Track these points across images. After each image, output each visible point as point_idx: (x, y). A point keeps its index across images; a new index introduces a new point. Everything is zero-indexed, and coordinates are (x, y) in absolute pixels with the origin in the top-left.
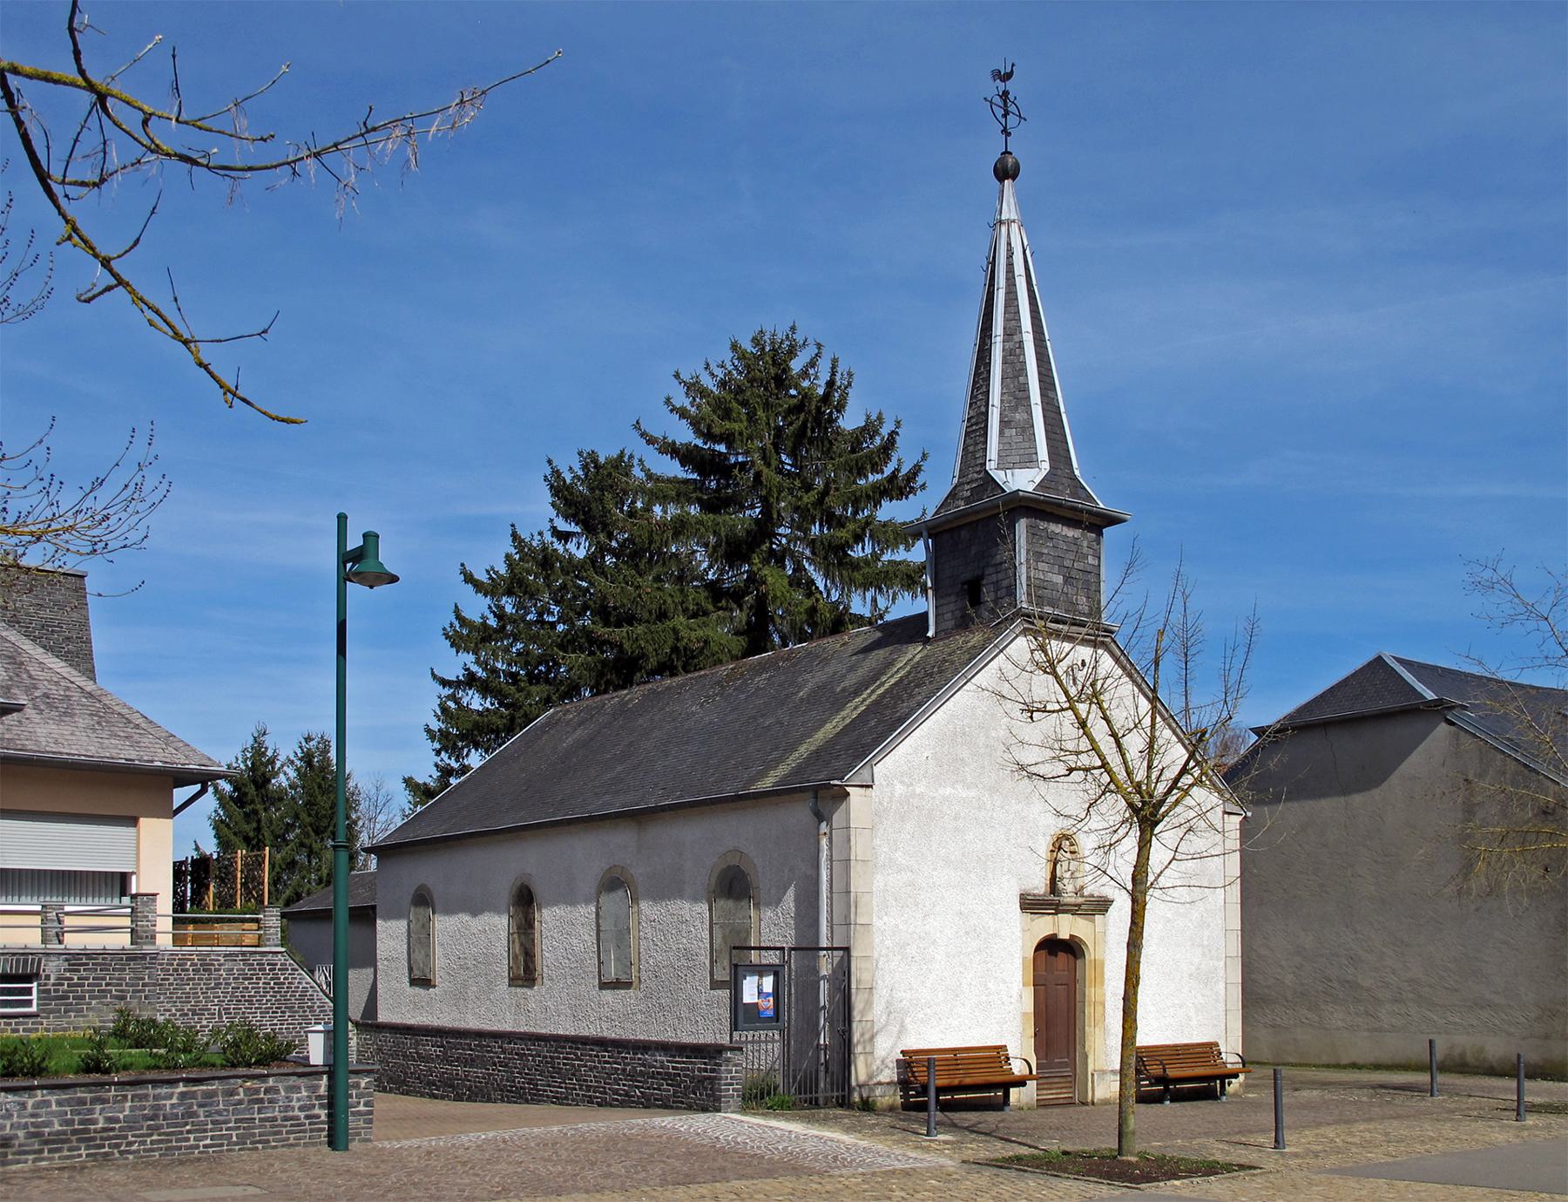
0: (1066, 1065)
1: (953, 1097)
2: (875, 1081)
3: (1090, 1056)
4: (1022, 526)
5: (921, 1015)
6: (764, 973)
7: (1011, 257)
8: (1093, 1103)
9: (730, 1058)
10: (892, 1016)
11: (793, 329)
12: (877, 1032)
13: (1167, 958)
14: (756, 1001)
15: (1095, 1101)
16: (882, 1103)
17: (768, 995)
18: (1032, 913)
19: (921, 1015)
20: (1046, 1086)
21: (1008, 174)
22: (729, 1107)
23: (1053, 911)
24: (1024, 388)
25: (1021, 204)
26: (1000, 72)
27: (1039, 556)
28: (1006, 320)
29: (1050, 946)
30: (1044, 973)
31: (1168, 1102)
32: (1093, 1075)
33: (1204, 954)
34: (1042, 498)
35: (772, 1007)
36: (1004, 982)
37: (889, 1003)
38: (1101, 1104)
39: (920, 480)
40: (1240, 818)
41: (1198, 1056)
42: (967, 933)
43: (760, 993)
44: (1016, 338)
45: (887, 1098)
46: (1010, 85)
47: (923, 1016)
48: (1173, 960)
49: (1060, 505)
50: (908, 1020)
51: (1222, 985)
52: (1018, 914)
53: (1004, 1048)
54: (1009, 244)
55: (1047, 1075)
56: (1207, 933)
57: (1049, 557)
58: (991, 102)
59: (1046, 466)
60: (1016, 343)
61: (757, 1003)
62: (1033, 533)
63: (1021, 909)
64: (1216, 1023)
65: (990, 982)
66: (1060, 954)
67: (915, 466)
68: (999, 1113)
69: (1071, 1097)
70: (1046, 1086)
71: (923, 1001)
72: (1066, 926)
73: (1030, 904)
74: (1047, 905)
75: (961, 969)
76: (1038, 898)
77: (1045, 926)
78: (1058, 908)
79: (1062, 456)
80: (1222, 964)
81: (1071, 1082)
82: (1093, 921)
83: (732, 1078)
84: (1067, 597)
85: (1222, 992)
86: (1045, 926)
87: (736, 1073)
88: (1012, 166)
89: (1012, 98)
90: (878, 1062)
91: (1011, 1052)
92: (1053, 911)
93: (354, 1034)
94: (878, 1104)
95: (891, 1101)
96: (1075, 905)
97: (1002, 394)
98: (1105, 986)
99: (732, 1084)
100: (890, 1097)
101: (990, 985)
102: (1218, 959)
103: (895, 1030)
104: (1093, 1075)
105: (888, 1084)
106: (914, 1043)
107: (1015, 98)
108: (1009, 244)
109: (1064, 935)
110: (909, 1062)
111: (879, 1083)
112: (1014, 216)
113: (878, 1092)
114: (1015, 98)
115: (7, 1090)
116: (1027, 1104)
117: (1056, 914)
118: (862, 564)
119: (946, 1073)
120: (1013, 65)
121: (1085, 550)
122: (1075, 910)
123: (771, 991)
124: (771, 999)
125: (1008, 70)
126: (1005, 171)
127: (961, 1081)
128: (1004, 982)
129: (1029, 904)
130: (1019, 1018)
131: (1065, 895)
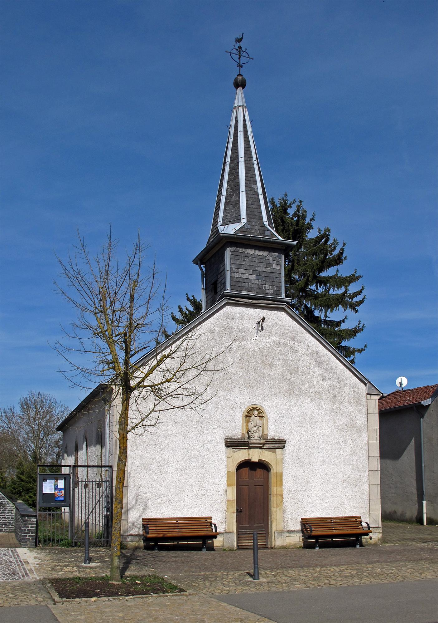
0: (262, 527)
1: (178, 543)
2: (129, 533)
3: (273, 523)
4: (228, 253)
5: (159, 501)
6: (59, 478)
7: (237, 123)
8: (275, 548)
9: (27, 520)
10: (139, 501)
11: (286, 195)
12: (130, 509)
13: (327, 471)
14: (54, 492)
15: (276, 546)
16: (131, 545)
17: (61, 489)
18: (233, 448)
19: (159, 501)
20: (247, 538)
21: (238, 84)
22: (27, 545)
23: (247, 447)
24: (238, 185)
25: (247, 98)
26: (238, 38)
27: (239, 266)
28: (232, 153)
29: (245, 465)
30: (248, 480)
31: (318, 548)
32: (275, 533)
33: (353, 469)
34: (236, 236)
35: (63, 495)
36: (214, 484)
37: (137, 495)
38: (279, 548)
39: (344, 255)
40: (379, 397)
41: (201, 524)
42: (190, 459)
43: (56, 488)
44: (235, 161)
45: (134, 543)
46: (242, 44)
47: (160, 501)
48: (332, 472)
49: (249, 240)
50: (150, 503)
51: (366, 486)
52: (224, 449)
53: (360, 517)
54: (236, 117)
55: (249, 533)
56: (356, 458)
57: (246, 266)
58: (249, 58)
59: (244, 221)
60: (235, 163)
61: (54, 493)
62: (235, 255)
63: (226, 447)
64: (362, 506)
65: (204, 483)
66: (258, 470)
67: (341, 249)
68: (199, 552)
69: (266, 545)
70: (247, 538)
71: (161, 493)
72: (255, 455)
73: (231, 443)
74: (235, 444)
75: (186, 477)
76: (234, 440)
77: (242, 455)
78: (249, 446)
79: (257, 216)
80: (366, 474)
81: (265, 536)
82: (275, 453)
83: (28, 530)
84: (259, 286)
85: (367, 490)
86: (242, 455)
87: (31, 528)
88: (240, 80)
89: (243, 49)
90: (130, 524)
91: (363, 520)
92: (247, 447)
93: (14, 508)
94: (129, 546)
95: (137, 544)
96: (261, 444)
97: (227, 189)
98: (283, 487)
99: (29, 533)
100: (137, 542)
101: (204, 485)
102: (364, 471)
103: (141, 508)
104: (275, 533)
105: (136, 535)
106: (153, 514)
107: (246, 49)
108: (236, 117)
109: (255, 459)
110: (147, 524)
111: (131, 535)
112: (240, 104)
113: (129, 539)
114: (246, 49)
115: (1, 532)
116: (228, 547)
117: (250, 449)
118: (320, 296)
119: (155, 531)
120: (243, 34)
121: (271, 262)
122: (261, 446)
123: (63, 487)
124: (63, 491)
125: (241, 37)
126: (240, 84)
127: (163, 536)
128: (214, 484)
129: (229, 444)
130: (224, 504)
131: (253, 438)
